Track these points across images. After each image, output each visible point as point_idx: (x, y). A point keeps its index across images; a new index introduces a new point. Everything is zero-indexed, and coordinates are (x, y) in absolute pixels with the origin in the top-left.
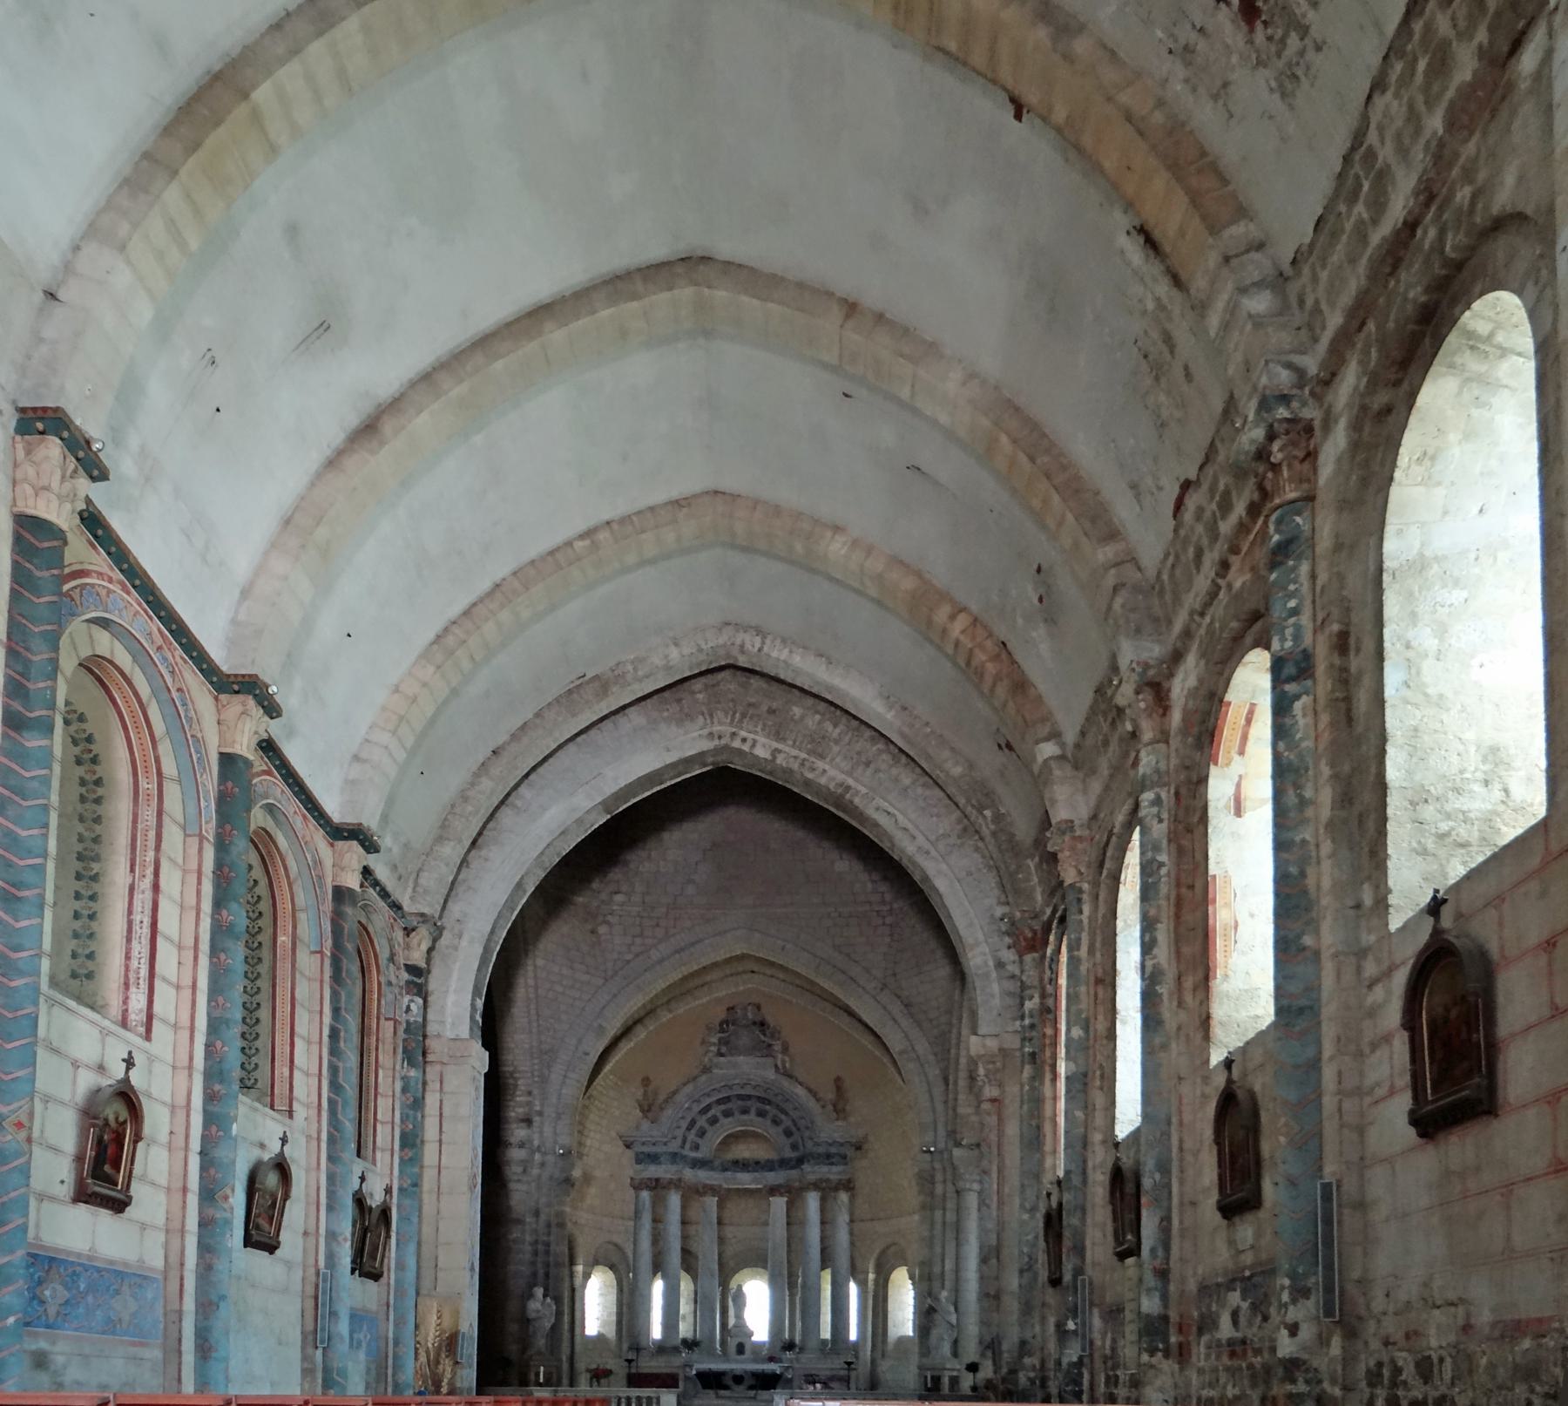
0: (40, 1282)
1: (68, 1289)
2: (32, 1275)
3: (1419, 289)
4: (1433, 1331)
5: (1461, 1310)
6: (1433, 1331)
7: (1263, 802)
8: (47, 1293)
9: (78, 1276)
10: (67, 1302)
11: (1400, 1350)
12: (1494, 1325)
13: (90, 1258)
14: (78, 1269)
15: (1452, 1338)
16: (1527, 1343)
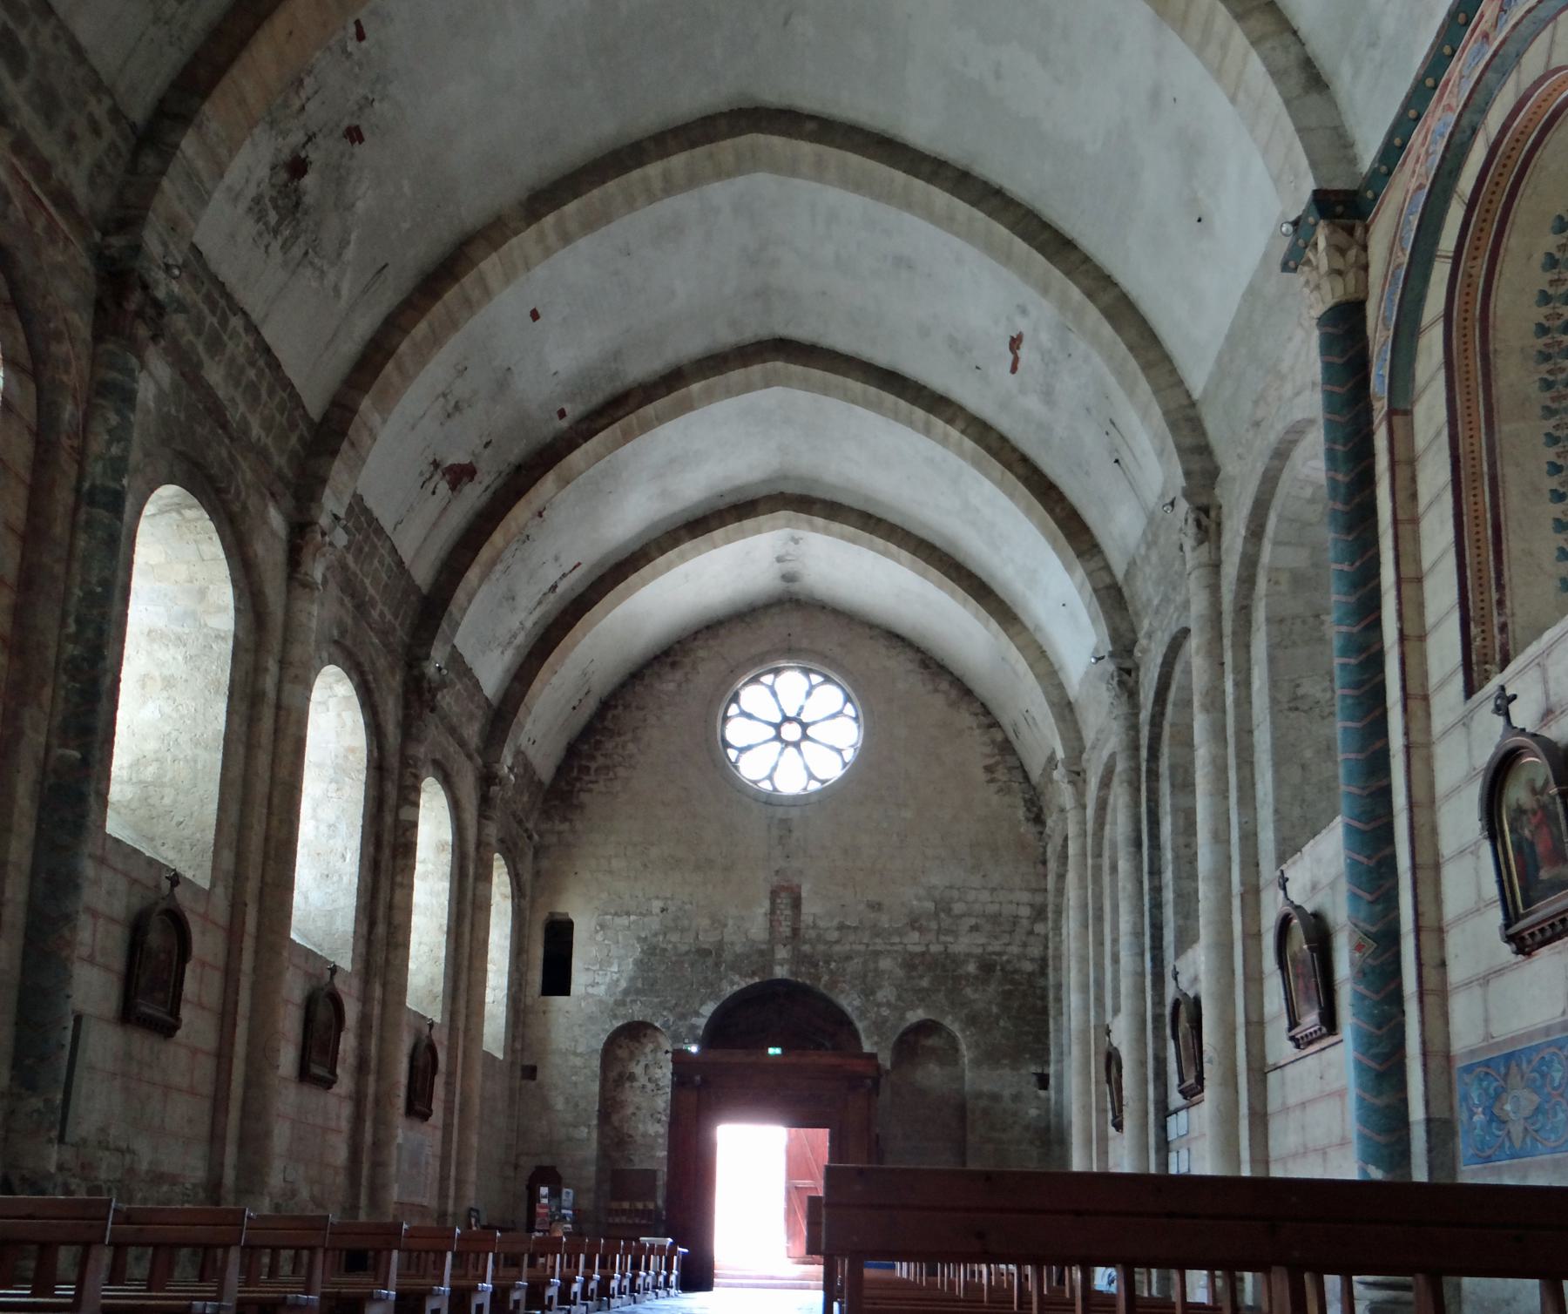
0: (1498, 1096)
1: (1536, 1091)
2: (1486, 1090)
3: (536, 815)
4: (104, 1166)
5: (128, 1157)
6: (104, 1166)
7: (424, 862)
8: (1508, 1107)
9: (1549, 1064)
10: (1537, 1110)
11: (74, 1176)
12: (147, 1172)
13: (1490, 1048)
14: (1546, 1054)
15: (118, 1175)
16: (165, 1188)
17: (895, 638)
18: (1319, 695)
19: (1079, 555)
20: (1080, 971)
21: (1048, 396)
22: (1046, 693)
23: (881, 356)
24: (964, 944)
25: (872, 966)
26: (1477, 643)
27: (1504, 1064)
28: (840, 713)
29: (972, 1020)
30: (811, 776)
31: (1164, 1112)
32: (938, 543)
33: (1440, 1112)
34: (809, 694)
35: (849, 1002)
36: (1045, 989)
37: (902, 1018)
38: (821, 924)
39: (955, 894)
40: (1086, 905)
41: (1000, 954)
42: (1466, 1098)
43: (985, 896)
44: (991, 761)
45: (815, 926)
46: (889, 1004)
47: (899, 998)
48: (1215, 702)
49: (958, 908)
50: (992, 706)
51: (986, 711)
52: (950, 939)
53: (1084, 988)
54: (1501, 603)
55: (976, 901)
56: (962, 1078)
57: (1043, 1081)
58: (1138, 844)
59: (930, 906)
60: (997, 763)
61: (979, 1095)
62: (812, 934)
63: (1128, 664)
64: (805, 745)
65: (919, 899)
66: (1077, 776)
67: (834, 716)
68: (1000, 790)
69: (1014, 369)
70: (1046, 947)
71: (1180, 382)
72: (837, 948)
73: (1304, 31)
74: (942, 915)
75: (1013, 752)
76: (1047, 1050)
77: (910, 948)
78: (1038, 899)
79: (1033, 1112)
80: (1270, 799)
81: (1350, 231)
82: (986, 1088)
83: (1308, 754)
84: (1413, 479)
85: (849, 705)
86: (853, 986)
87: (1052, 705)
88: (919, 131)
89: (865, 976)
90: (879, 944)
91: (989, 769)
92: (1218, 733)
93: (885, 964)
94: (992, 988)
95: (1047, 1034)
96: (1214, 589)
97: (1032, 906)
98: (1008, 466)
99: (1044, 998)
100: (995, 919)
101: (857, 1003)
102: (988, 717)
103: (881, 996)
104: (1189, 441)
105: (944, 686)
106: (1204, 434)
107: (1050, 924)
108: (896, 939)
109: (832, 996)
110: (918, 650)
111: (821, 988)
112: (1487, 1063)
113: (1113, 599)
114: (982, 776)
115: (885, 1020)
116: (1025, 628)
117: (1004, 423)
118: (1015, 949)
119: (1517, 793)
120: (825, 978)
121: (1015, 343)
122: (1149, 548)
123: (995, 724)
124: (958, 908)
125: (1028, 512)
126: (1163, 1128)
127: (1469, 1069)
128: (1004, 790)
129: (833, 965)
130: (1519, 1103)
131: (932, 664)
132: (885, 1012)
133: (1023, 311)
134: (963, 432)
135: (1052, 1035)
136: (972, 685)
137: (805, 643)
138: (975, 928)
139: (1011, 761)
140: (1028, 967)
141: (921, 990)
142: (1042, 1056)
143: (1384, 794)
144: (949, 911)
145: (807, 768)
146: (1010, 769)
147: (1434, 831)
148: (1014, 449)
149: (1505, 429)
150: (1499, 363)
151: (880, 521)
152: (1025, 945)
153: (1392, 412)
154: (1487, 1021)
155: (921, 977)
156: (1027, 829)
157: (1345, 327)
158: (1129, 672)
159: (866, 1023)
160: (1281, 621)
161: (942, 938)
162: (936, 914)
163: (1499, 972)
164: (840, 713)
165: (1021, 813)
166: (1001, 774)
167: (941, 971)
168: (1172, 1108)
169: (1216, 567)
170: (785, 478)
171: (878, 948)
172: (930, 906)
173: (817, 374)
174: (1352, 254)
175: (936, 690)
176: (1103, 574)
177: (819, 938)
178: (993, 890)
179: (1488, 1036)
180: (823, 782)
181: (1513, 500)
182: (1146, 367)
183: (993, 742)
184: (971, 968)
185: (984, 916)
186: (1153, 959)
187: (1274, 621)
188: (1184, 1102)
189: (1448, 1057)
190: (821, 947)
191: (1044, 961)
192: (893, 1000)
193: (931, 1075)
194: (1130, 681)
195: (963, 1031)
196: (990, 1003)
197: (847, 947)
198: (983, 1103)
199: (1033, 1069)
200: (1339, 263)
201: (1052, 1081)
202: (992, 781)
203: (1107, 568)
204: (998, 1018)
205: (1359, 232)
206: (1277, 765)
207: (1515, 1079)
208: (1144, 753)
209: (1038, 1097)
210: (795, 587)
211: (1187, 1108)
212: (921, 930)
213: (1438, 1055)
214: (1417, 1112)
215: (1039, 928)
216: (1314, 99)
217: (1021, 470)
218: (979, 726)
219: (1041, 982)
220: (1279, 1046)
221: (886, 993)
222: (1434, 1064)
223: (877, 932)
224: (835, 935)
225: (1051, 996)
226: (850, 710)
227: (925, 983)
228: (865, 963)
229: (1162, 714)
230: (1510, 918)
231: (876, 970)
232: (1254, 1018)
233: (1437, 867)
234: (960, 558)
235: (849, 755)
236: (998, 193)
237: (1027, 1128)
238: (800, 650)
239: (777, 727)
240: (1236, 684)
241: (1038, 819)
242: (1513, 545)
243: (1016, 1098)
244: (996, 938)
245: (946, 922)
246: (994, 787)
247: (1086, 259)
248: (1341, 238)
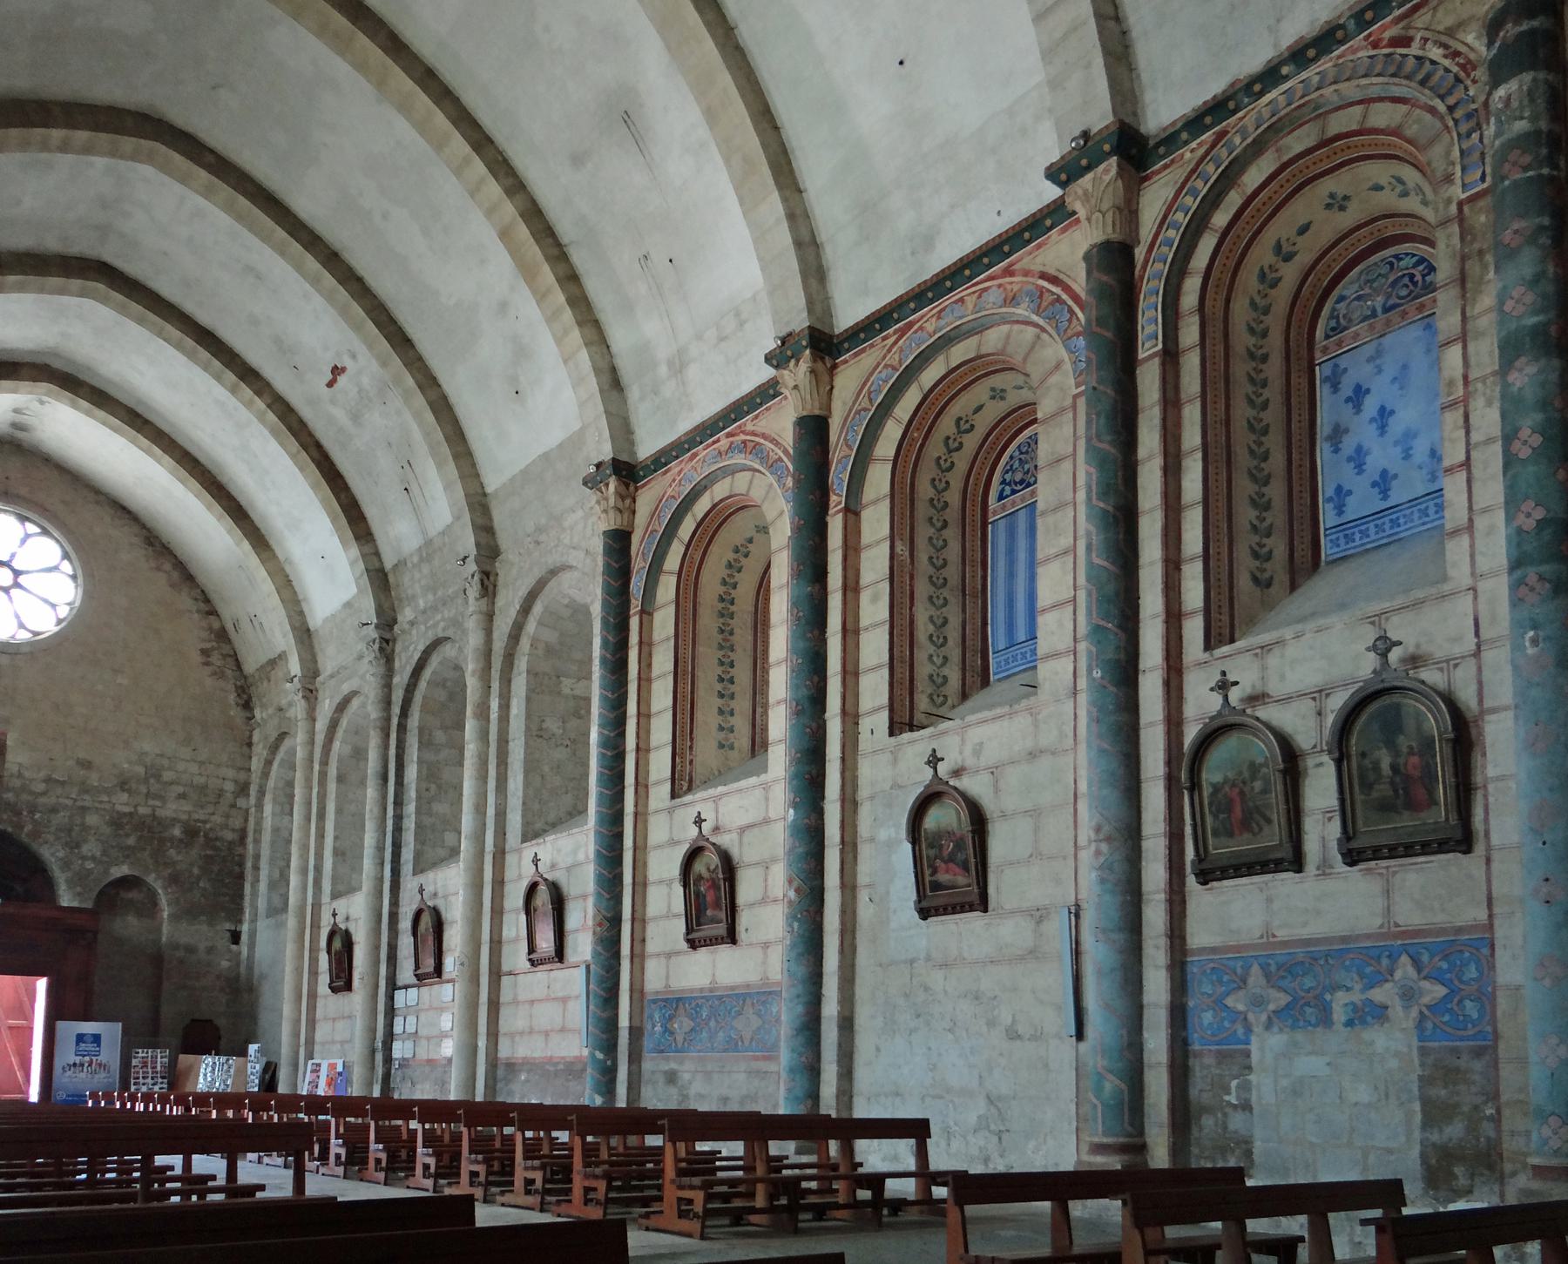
0: (671, 1018)
14: (700, 1002)
17: (122, 510)
18: (555, 730)
19: (357, 538)
20: (301, 856)
21: (356, 418)
22: (289, 617)
23: (205, 318)
24: (171, 809)
25: (78, 821)
26: (678, 768)
27: (674, 1003)
28: (56, 568)
29: (174, 880)
30: (22, 626)
31: (393, 986)
32: (202, 460)
33: (636, 1023)
34: (23, 541)
35: (51, 854)
36: (242, 857)
37: (106, 872)
38: (27, 774)
39: (166, 762)
40: (310, 803)
41: (205, 822)
42: (651, 1017)
43: (194, 768)
44: (208, 645)
45: (20, 775)
46: (93, 858)
47: (104, 853)
48: (483, 713)
49: (168, 776)
50: (213, 596)
51: (207, 600)
52: (158, 803)
53: (304, 871)
54: (691, 748)
55: (185, 772)
56: (159, 930)
57: (236, 937)
58: (385, 779)
59: (141, 770)
60: (213, 649)
61: (176, 947)
62: (17, 783)
63: (388, 636)
64: (14, 592)
65: (130, 763)
66: (310, 694)
67: (50, 570)
68: (214, 674)
69: (330, 384)
70: (246, 820)
71: (478, 475)
72: (42, 800)
73: (614, 349)
74: (152, 781)
75: (229, 641)
76: (241, 910)
77: (119, 808)
78: (242, 776)
79: (225, 964)
80: (520, 794)
81: (627, 486)
82: (184, 940)
83: (546, 769)
84: (650, 655)
85: (66, 562)
86: (58, 838)
87: (294, 628)
88: (304, 205)
89: (70, 830)
90: (87, 801)
91: (205, 652)
92: (484, 735)
93: (92, 820)
94: (194, 852)
95: (241, 896)
96: (489, 632)
97: (236, 782)
98: (305, 447)
99: (241, 864)
100: (203, 789)
101: (61, 854)
102: (208, 606)
103: (86, 849)
104: (480, 521)
105: (168, 566)
106: (491, 519)
107: (253, 800)
108: (106, 799)
109: (34, 846)
110: (144, 526)
111: (24, 838)
112: (665, 1000)
113: (380, 579)
114: (199, 659)
115: (90, 872)
116: (275, 556)
117: (306, 412)
118: (217, 819)
119: (699, 867)
120: (28, 828)
121: (337, 371)
122: (421, 560)
123: (213, 612)
124: (168, 776)
125: (315, 487)
126: (390, 998)
127: (655, 1001)
128: (219, 674)
129: (37, 816)
130: (682, 1025)
131: (156, 544)
132: (90, 865)
133: (354, 357)
134: (269, 406)
135: (247, 899)
136: (194, 571)
137: (23, 491)
138: (182, 796)
139: (226, 649)
140: (229, 836)
141: (129, 847)
142: (236, 913)
143: (619, 836)
144: (158, 777)
145: (17, 616)
146: (225, 656)
147: (645, 864)
148: (311, 435)
149: (701, 649)
150: (701, 610)
151: (146, 422)
152: (227, 816)
153: (643, 612)
154: (667, 978)
155: (127, 835)
156: (236, 713)
157: (619, 543)
158: (387, 641)
159: (69, 874)
160: (536, 674)
161: (151, 802)
162: (146, 781)
163: (678, 953)
164: (56, 568)
165: (232, 697)
166: (216, 659)
167: (150, 831)
168: (400, 983)
169: (490, 616)
170: (56, 355)
171: (86, 804)
172: (141, 770)
173: (137, 308)
174: (628, 501)
175: (158, 569)
176: (375, 559)
177: (24, 789)
178: (202, 763)
179: (667, 986)
180: (36, 634)
181: (701, 692)
182: (456, 457)
183: (211, 629)
184: (177, 832)
185: (192, 785)
186: (393, 870)
187: (532, 673)
188: (414, 981)
189: (642, 991)
190: (25, 797)
191: (243, 834)
192: (98, 854)
193: (129, 926)
194: (389, 649)
195: (165, 888)
196: (192, 865)
197: (53, 800)
198: (180, 954)
199: (228, 926)
200: (620, 505)
201: (244, 938)
202: (207, 664)
203: (377, 554)
204: (199, 878)
205: (632, 488)
206: (527, 772)
207: (681, 1011)
208: (396, 710)
209: (230, 951)
210: (20, 435)
211: (418, 986)
212: (129, 791)
213: (637, 991)
214: (624, 1021)
215: (241, 803)
216: (615, 393)
217: (316, 454)
218: (198, 611)
219: (239, 850)
220: (515, 957)
221: (91, 848)
222: (636, 996)
223: (85, 789)
224: (41, 787)
225: (249, 864)
226: (67, 567)
227: (131, 841)
228: (70, 817)
229: (415, 685)
230: (689, 930)
231: (83, 824)
232: (496, 938)
233: (645, 885)
234: (223, 479)
235: (64, 612)
236: (360, 280)
237: (218, 977)
238: (18, 496)
239: (17, 585)
240: (500, 707)
241: (247, 706)
242: (698, 715)
243: (210, 950)
244: (202, 807)
245: (155, 786)
246: (208, 670)
247: (420, 359)
248: (622, 489)
